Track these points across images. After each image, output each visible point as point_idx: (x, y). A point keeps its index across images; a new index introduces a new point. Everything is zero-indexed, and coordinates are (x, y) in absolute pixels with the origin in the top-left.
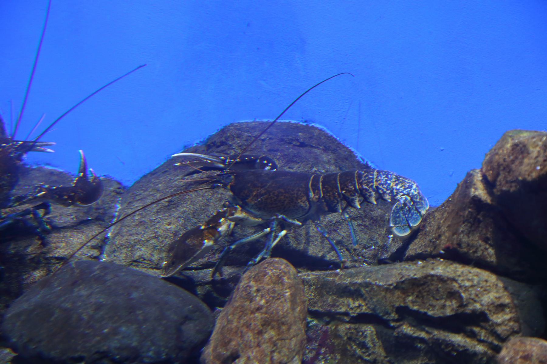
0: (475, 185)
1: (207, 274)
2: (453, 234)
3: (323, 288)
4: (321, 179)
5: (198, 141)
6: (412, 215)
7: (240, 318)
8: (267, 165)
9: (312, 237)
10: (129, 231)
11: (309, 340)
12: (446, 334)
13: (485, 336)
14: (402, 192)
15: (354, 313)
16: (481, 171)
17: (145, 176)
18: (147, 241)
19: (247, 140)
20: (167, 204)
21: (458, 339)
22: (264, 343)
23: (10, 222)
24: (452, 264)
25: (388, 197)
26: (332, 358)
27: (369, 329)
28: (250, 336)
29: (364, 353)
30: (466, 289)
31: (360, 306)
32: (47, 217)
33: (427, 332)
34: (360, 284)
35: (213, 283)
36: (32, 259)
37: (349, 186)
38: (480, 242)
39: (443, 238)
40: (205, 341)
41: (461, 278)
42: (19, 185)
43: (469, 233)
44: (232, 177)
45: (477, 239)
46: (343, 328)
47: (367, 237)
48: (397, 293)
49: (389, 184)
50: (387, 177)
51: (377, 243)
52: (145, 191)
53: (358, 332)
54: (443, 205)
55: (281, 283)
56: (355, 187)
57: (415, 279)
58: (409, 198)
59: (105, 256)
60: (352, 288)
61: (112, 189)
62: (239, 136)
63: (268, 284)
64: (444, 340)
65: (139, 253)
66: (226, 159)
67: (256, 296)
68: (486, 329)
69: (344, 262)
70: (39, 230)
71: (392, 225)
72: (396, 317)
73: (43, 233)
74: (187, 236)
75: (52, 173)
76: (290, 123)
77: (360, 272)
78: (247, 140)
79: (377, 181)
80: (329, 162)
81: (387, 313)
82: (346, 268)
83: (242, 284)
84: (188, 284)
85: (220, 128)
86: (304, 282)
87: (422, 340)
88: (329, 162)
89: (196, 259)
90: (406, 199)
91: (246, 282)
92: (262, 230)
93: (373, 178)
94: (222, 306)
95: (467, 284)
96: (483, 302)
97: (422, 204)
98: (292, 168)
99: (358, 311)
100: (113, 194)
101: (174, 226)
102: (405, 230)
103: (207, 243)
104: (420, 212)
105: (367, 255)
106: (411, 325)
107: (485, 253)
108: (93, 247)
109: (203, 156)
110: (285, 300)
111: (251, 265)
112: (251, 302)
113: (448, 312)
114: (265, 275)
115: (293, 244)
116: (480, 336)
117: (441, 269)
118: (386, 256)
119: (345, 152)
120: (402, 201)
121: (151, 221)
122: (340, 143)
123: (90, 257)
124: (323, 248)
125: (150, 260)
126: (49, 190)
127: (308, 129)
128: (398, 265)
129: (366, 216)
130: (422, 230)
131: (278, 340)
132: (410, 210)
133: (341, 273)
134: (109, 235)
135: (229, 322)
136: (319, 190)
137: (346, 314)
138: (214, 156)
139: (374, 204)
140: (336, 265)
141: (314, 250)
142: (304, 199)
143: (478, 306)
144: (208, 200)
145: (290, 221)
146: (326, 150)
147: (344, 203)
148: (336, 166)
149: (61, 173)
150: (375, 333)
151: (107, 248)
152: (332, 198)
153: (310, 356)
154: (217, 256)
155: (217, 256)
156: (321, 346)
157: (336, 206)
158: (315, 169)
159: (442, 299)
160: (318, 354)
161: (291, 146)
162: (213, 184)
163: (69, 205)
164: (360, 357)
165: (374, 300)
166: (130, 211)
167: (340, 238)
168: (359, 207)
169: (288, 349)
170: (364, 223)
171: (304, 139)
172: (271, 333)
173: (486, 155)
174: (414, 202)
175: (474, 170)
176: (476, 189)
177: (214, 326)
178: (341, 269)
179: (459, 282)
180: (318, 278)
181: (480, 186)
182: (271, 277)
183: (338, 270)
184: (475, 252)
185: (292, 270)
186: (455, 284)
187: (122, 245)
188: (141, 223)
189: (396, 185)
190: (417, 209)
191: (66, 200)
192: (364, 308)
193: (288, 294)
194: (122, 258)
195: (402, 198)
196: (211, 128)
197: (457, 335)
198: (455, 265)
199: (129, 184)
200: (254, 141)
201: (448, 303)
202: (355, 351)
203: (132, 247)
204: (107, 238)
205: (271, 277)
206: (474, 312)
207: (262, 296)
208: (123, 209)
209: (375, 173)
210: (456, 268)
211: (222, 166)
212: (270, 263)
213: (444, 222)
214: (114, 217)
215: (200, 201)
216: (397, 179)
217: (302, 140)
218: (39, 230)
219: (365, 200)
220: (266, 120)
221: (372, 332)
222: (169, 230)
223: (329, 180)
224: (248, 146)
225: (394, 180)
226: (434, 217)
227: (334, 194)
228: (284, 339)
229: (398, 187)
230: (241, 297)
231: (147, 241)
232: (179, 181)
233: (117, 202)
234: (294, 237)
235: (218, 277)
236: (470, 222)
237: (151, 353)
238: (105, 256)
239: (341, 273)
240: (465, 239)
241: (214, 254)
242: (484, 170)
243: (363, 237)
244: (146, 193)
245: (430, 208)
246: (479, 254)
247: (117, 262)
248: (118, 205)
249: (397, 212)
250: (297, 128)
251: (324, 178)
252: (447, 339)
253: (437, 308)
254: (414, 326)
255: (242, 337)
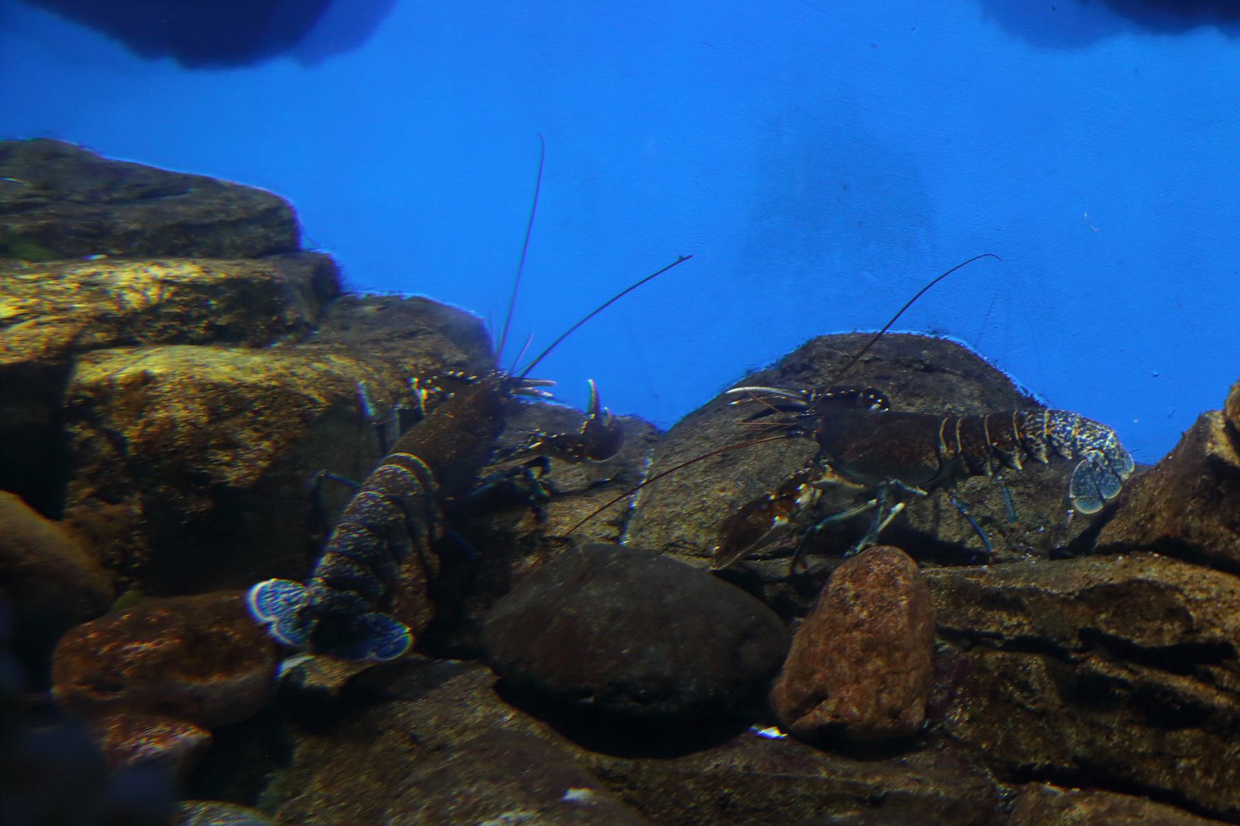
0: (1212, 436)
1: (783, 566)
2: (1176, 515)
3: (960, 594)
4: (958, 425)
5: (768, 364)
6: (1107, 481)
7: (828, 637)
8: (874, 401)
9: (944, 511)
10: (663, 499)
11: (938, 673)
12: (1164, 675)
13: (1230, 682)
14: (1090, 444)
15: (1009, 636)
16: (1224, 413)
17: (689, 416)
18: (690, 515)
19: (841, 362)
20: (719, 459)
21: (1183, 684)
22: (866, 677)
23: (491, 485)
24: (1173, 563)
25: (1067, 453)
26: (974, 704)
27: (1035, 662)
28: (844, 666)
29: (1025, 698)
30: (1198, 604)
31: (1019, 625)
32: (546, 476)
33: (1131, 671)
34: (1020, 591)
35: (793, 579)
36: (524, 540)
37: (1001, 430)
38: (1222, 529)
39: (1158, 519)
40: (775, 671)
41: (1189, 587)
42: (510, 429)
43: (1203, 513)
44: (819, 420)
45: (1216, 523)
46: (992, 657)
47: (1031, 512)
48: (1082, 608)
49: (1070, 432)
50: (1065, 420)
51: (1048, 522)
52: (688, 439)
53: (1018, 665)
54: (1158, 466)
55: (894, 585)
56: (1013, 436)
57: (1112, 586)
58: (1102, 455)
59: (628, 536)
60: (1007, 596)
61: (641, 434)
62: (830, 356)
63: (873, 587)
64: (1159, 686)
65: (677, 533)
66: (810, 393)
67: (854, 605)
68: (1231, 670)
69: (993, 554)
70: (532, 498)
71: (1071, 496)
72: (1080, 645)
73: (535, 500)
74: (747, 510)
75: (555, 411)
76: (909, 334)
77: (1021, 572)
78: (841, 362)
79: (1049, 427)
80: (971, 396)
81: (1064, 638)
82: (999, 561)
83: (832, 585)
84: (748, 581)
85: (802, 343)
86: (929, 583)
87: (1123, 684)
88: (971, 396)
89: (761, 545)
90: (1097, 456)
91: (839, 582)
92: (866, 502)
93: (1042, 423)
94: (803, 616)
95: (1200, 596)
96: (1226, 627)
97: (1123, 463)
98: (912, 405)
99: (1017, 632)
100: (643, 442)
101: (730, 494)
102: (1093, 505)
103: (779, 521)
104: (1120, 478)
105: (1032, 540)
106: (1103, 659)
107: (1231, 547)
108: (611, 523)
109: (774, 390)
110: (900, 612)
111: (849, 556)
112: (846, 613)
113: (1167, 641)
114: (868, 573)
115: (914, 522)
116: (1222, 681)
117: (1154, 570)
118: (1062, 543)
119: (997, 378)
120: (1090, 459)
121: (697, 485)
122: (988, 366)
123: (607, 538)
124: (962, 529)
125: (694, 544)
126: (547, 440)
127: (937, 345)
128: (1083, 562)
129: (1030, 480)
130: (1123, 505)
131: (888, 673)
132: (1102, 473)
133: (990, 571)
134: (634, 505)
135: (812, 643)
136: (955, 440)
137: (997, 636)
138: (791, 389)
139: (1044, 464)
140: (981, 557)
141: (948, 532)
142: (932, 454)
143: (1218, 632)
144: (781, 453)
145: (909, 488)
146: (967, 376)
147: (997, 463)
148: (982, 402)
149: (569, 411)
150: (1044, 668)
151: (631, 524)
152: (976, 454)
153: (940, 698)
154: (794, 539)
155: (794, 539)
156: (956, 684)
157: (982, 465)
158: (948, 406)
159: (1156, 619)
160: (952, 696)
161: (910, 370)
162: (789, 431)
163: (574, 462)
164: (1020, 705)
165: (1044, 617)
166: (665, 470)
167: (989, 514)
168: (1020, 467)
169: (904, 688)
170: (1027, 491)
171: (929, 361)
172: (876, 663)
173: (1232, 388)
174: (1110, 461)
175: (1211, 412)
176: (1215, 443)
177: (789, 648)
178: (990, 565)
179: (1186, 592)
180: (952, 578)
181: (1222, 438)
182: (877, 575)
183: (985, 567)
184: (1213, 545)
185: (911, 565)
186: (1178, 596)
187: (653, 520)
188: (682, 488)
189: (1081, 433)
190: (1114, 472)
191: (571, 453)
192: (1026, 628)
193: (904, 603)
194: (652, 539)
195: (1090, 454)
196: (785, 343)
197: (1181, 679)
198: (1178, 565)
199: (667, 427)
200: (851, 364)
201: (1167, 626)
202: (1011, 694)
203: (667, 523)
204: (632, 509)
205: (877, 575)
206: (1211, 641)
207: (863, 606)
208: (655, 466)
209: (1046, 414)
210: (1180, 569)
211: (803, 403)
212: (876, 555)
213: (1160, 493)
214: (642, 477)
215: (770, 455)
216: (1083, 423)
217: (927, 362)
218: (532, 498)
219: (1030, 457)
220: (872, 331)
221: (1039, 667)
222: (722, 499)
223: (971, 426)
224: (842, 371)
225: (1076, 425)
226: (1143, 485)
227: (979, 447)
228: (898, 673)
229: (1084, 437)
230: (830, 606)
231: (690, 515)
232: (738, 423)
233: (648, 455)
234: (916, 512)
235: (800, 570)
236: (1204, 497)
237: (691, 688)
238: (628, 536)
239: (990, 571)
240: (1196, 524)
241: (791, 536)
242: (1228, 414)
243: (1025, 513)
244: (689, 442)
245: (1136, 466)
246: (1220, 548)
247: (646, 546)
248: (649, 460)
249: (1082, 475)
250: (919, 342)
251: (963, 422)
252: (1165, 684)
253: (1148, 633)
254: (1109, 661)
255: (832, 667)
